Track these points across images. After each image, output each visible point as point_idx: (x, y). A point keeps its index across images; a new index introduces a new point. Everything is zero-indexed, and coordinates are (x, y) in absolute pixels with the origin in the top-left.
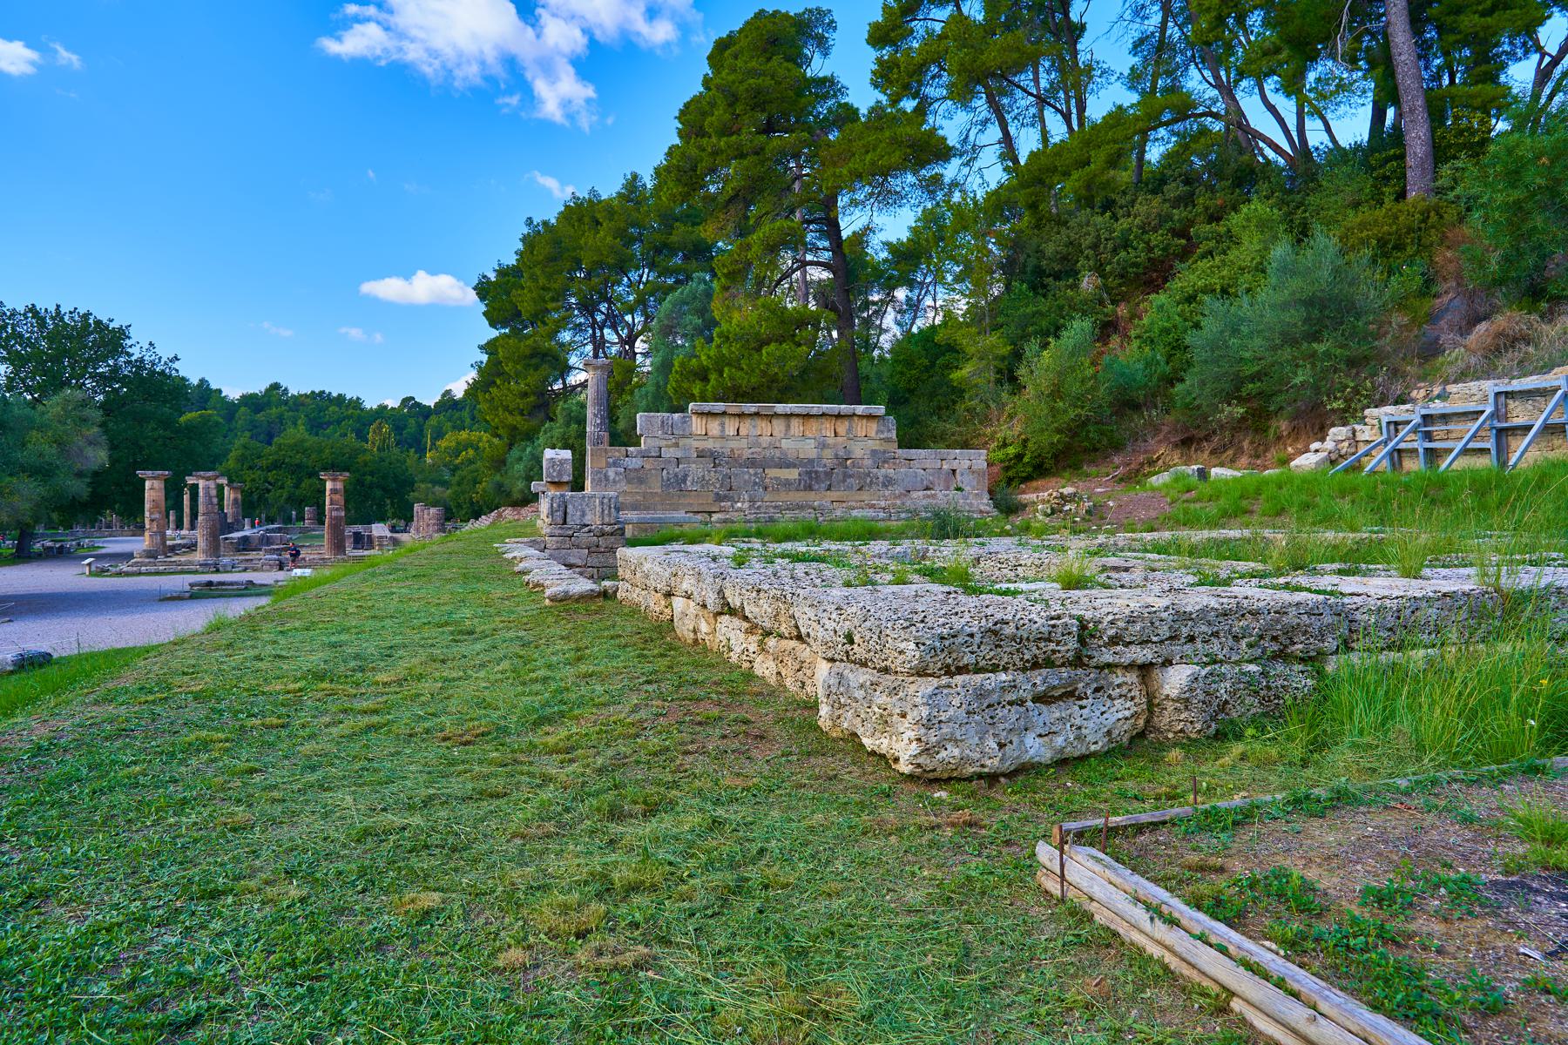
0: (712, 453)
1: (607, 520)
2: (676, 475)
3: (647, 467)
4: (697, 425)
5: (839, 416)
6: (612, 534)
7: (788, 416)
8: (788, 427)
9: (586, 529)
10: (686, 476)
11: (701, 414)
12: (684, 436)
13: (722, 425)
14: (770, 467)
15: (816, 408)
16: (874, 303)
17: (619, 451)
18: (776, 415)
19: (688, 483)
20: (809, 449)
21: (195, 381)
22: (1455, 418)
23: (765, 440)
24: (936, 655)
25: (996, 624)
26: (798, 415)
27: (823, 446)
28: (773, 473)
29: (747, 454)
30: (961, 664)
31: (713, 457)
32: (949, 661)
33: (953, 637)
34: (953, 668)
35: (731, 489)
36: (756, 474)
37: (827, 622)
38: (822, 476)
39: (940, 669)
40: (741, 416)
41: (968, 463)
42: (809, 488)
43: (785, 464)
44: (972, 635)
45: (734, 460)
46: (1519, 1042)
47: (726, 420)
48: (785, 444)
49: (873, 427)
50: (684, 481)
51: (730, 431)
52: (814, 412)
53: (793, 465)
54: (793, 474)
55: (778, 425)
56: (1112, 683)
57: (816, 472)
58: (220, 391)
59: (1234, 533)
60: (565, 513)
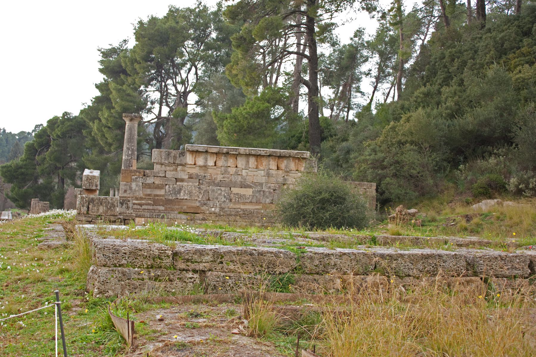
0: (197, 175)
2: (174, 188)
4: (189, 159)
5: (280, 157)
8: (248, 162)
11: (192, 152)
13: (206, 160)
14: (234, 187)
15: (262, 151)
16: (262, 47)
18: (240, 155)
19: (182, 194)
21: (98, 93)
24: (110, 259)
26: (254, 155)
28: (235, 190)
29: (220, 178)
30: (121, 264)
32: (116, 262)
34: (117, 265)
35: (209, 200)
36: (225, 191)
38: (267, 194)
44: (125, 253)
45: (212, 182)
46: (8, 356)
47: (209, 157)
50: (179, 192)
51: (211, 163)
52: (263, 153)
53: (250, 187)
55: (241, 162)
56: (186, 277)
57: (264, 191)
58: (11, 133)
59: (149, 202)
60: (88, 208)
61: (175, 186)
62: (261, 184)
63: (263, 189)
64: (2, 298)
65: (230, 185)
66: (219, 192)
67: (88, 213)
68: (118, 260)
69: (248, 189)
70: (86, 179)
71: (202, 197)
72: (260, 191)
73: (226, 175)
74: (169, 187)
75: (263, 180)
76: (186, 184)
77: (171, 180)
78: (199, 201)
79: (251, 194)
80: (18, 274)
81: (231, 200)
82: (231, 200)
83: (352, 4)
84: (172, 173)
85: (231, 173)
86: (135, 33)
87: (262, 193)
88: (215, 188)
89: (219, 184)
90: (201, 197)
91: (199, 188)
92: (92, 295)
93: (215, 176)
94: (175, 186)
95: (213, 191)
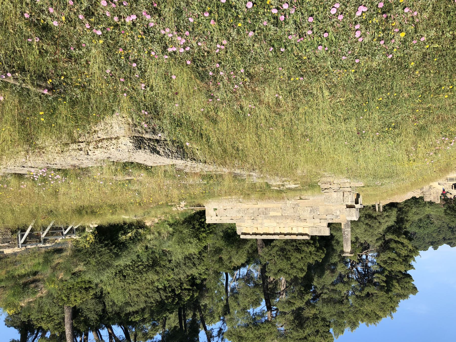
6: (325, 189)
7: (274, 234)
9: (335, 190)
12: (312, 227)
23: (282, 225)
27: (262, 224)
29: (288, 221)
36: (285, 213)
42: (266, 209)
50: (311, 211)
53: (271, 217)
54: (272, 214)
57: (264, 214)
61: (314, 214)
62: (265, 218)
64: (455, 167)
65: (282, 217)
67: (343, 192)
69: (272, 215)
70: (353, 214)
72: (266, 214)
73: (285, 222)
74: (317, 213)
75: (265, 221)
77: (317, 217)
79: (270, 213)
80: (299, 92)
83: (190, 324)
85: (282, 224)
86: (435, 248)
87: (265, 213)
90: (298, 209)
92: (212, 40)
93: (291, 221)
94: (314, 214)
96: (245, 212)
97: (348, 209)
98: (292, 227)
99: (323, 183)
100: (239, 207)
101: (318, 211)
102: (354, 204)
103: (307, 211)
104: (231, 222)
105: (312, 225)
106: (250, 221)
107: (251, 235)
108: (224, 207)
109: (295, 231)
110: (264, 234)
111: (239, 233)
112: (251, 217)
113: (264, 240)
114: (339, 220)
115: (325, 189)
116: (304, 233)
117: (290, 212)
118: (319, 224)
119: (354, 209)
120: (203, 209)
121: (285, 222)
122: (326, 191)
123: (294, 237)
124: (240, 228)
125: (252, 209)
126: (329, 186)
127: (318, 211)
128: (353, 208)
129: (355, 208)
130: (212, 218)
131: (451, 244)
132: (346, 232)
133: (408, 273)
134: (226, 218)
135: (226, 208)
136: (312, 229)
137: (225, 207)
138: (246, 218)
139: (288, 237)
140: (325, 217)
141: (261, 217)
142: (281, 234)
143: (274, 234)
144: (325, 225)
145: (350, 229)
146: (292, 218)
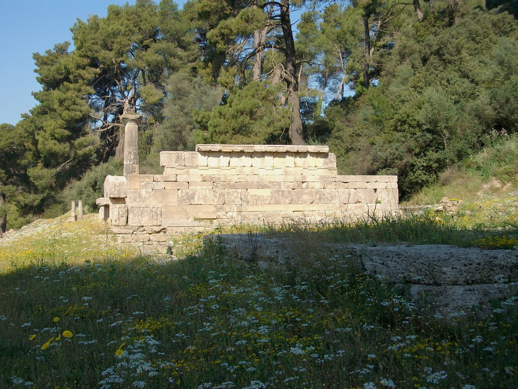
0: (211, 178)
1: (155, 223)
3: (168, 188)
4: (202, 160)
9: (142, 229)
10: (194, 194)
17: (149, 178)
19: (196, 199)
20: (277, 176)
22: (267, 154)
23: (248, 170)
25: (490, 258)
27: (286, 173)
29: (235, 179)
31: (213, 181)
33: (470, 264)
34: (470, 282)
37: (390, 263)
38: (286, 193)
39: (464, 282)
40: (231, 154)
41: (385, 185)
42: (277, 203)
43: (262, 186)
45: (228, 185)
48: (261, 172)
49: (320, 161)
50: (193, 198)
53: (267, 187)
54: (266, 193)
57: (282, 191)
62: (279, 184)
63: (282, 189)
66: (235, 194)
68: (471, 275)
69: (266, 190)
71: (218, 201)
72: (279, 191)
73: (242, 176)
74: (182, 192)
75: (281, 179)
76: (199, 187)
77: (183, 185)
78: (215, 206)
79: (269, 194)
81: (248, 202)
82: (248, 202)
84: (185, 176)
87: (280, 193)
88: (231, 191)
89: (235, 186)
90: (216, 201)
91: (214, 191)
93: (230, 178)
94: (188, 190)
95: (229, 193)
96: (318, 196)
97: (122, 196)
98: (229, 168)
99: (162, 243)
100: (330, 205)
101: (180, 196)
102: (111, 206)
103: (201, 196)
104: (347, 176)
105: (192, 171)
106: (309, 179)
107: (308, 152)
108: (361, 207)
109: (224, 160)
110: (283, 154)
111: (332, 156)
112: (307, 187)
113: (288, 141)
114: (142, 180)
115: (159, 232)
116: (277, 159)
117: (235, 195)
118: (179, 172)
119: (112, 196)
120: (404, 203)
121: (242, 176)
122: (157, 229)
123: (247, 148)
124: (330, 165)
125: (305, 202)
126: (152, 237)
127: (180, 196)
128: (114, 198)
129: (110, 198)
130: (384, 185)
131: (5, 127)
132: (132, 157)
133: (159, 4)
134: (358, 185)
135: (358, 204)
136: (193, 162)
137: (359, 207)
138: (318, 186)
139: (217, 147)
140: (169, 186)
141: (288, 186)
142: (252, 155)
143: (263, 154)
144: (167, 172)
145: (125, 163)
146: (229, 184)
